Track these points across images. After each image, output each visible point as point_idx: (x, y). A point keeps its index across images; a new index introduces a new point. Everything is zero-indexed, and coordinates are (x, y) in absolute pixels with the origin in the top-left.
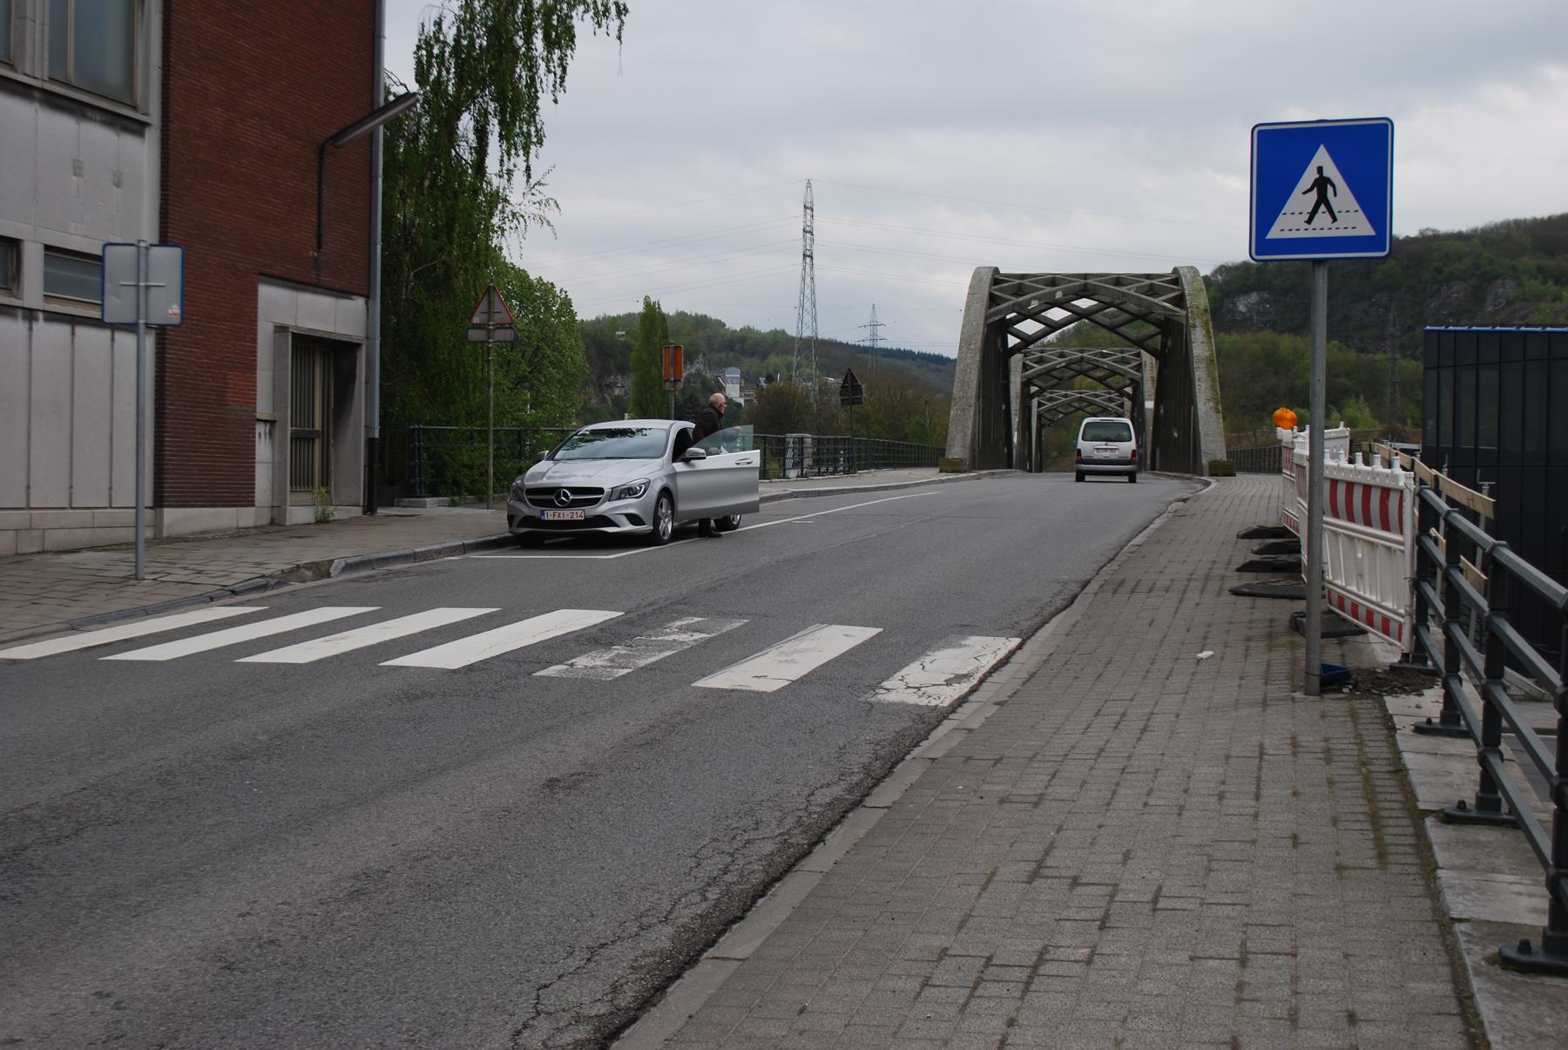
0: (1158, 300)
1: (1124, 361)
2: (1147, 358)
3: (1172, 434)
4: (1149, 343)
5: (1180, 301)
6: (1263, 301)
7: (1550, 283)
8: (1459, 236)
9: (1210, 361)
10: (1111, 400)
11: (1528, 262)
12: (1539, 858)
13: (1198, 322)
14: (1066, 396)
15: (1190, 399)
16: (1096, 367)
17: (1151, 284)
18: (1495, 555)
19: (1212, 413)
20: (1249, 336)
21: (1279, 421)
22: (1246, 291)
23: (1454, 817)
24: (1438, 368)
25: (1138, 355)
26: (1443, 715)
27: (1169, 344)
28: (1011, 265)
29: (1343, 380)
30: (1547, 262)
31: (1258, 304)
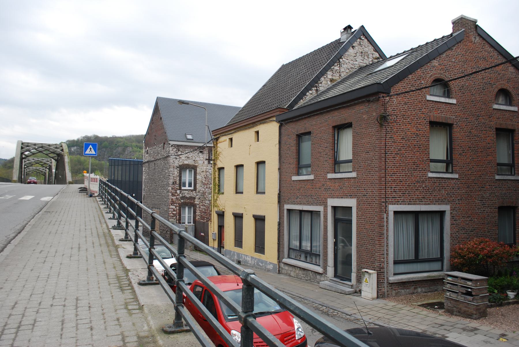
0: (58, 150)
1: (48, 161)
2: (53, 161)
3: (59, 176)
4: (54, 158)
5: (62, 150)
6: (77, 149)
7: (139, 148)
8: (121, 138)
9: (69, 162)
10: (43, 169)
11: (134, 144)
12: (201, 344)
13: (66, 155)
14: (33, 168)
15: (64, 169)
16: (41, 162)
17: (56, 146)
18: (180, 234)
19: (69, 172)
20: (74, 156)
21: (84, 172)
22: (73, 146)
23: (142, 284)
24: (111, 165)
25: (51, 160)
26: (117, 225)
27: (59, 158)
28: (25, 141)
29: (95, 167)
30: (138, 144)
31: (76, 149)
